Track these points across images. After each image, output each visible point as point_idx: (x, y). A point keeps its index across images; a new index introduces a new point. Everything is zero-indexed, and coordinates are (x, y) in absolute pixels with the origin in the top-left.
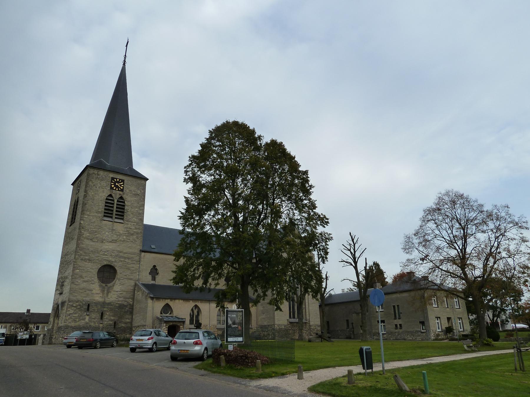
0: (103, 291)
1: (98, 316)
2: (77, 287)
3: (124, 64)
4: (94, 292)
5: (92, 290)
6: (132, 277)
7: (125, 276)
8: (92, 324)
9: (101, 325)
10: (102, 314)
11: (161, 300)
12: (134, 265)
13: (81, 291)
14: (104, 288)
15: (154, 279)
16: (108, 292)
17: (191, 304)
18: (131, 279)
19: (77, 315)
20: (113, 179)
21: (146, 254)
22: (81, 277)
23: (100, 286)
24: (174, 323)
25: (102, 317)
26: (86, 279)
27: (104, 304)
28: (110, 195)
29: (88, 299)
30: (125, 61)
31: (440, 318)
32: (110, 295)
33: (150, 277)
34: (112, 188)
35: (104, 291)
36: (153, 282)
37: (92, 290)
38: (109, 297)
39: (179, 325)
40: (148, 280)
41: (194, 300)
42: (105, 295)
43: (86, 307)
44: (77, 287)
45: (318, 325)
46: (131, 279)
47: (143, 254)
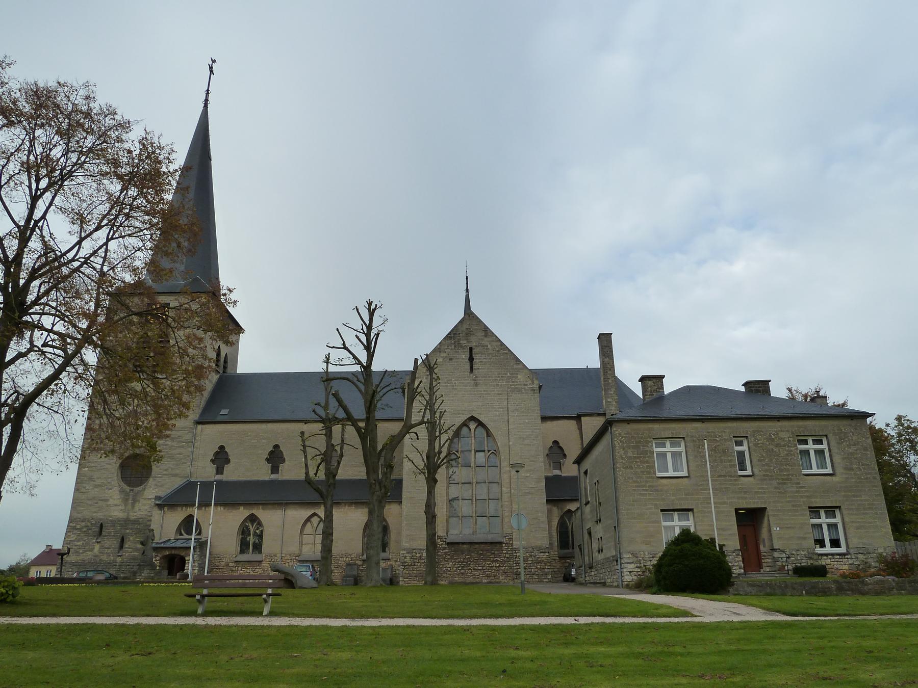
0: (125, 500)
1: (116, 543)
2: (84, 497)
3: (206, 106)
4: (111, 502)
5: (107, 500)
6: (177, 472)
7: (166, 470)
8: (104, 558)
9: (119, 560)
10: (123, 540)
11: (179, 509)
12: (181, 450)
13: (90, 502)
14: (127, 494)
15: (275, 470)
16: (135, 501)
17: (242, 513)
18: (175, 475)
19: (80, 543)
21: (204, 426)
22: (91, 479)
23: (122, 491)
24: (173, 552)
25: (121, 546)
26: (98, 482)
27: (126, 522)
29: (99, 515)
30: (206, 100)
31: (839, 507)
32: (138, 506)
33: (212, 468)
35: (127, 500)
36: (274, 476)
37: (107, 500)
38: (136, 509)
39: (183, 554)
41: (247, 505)
42: (130, 507)
43: (98, 529)
44: (84, 497)
45: (540, 550)
46: (175, 475)
47: (200, 427)
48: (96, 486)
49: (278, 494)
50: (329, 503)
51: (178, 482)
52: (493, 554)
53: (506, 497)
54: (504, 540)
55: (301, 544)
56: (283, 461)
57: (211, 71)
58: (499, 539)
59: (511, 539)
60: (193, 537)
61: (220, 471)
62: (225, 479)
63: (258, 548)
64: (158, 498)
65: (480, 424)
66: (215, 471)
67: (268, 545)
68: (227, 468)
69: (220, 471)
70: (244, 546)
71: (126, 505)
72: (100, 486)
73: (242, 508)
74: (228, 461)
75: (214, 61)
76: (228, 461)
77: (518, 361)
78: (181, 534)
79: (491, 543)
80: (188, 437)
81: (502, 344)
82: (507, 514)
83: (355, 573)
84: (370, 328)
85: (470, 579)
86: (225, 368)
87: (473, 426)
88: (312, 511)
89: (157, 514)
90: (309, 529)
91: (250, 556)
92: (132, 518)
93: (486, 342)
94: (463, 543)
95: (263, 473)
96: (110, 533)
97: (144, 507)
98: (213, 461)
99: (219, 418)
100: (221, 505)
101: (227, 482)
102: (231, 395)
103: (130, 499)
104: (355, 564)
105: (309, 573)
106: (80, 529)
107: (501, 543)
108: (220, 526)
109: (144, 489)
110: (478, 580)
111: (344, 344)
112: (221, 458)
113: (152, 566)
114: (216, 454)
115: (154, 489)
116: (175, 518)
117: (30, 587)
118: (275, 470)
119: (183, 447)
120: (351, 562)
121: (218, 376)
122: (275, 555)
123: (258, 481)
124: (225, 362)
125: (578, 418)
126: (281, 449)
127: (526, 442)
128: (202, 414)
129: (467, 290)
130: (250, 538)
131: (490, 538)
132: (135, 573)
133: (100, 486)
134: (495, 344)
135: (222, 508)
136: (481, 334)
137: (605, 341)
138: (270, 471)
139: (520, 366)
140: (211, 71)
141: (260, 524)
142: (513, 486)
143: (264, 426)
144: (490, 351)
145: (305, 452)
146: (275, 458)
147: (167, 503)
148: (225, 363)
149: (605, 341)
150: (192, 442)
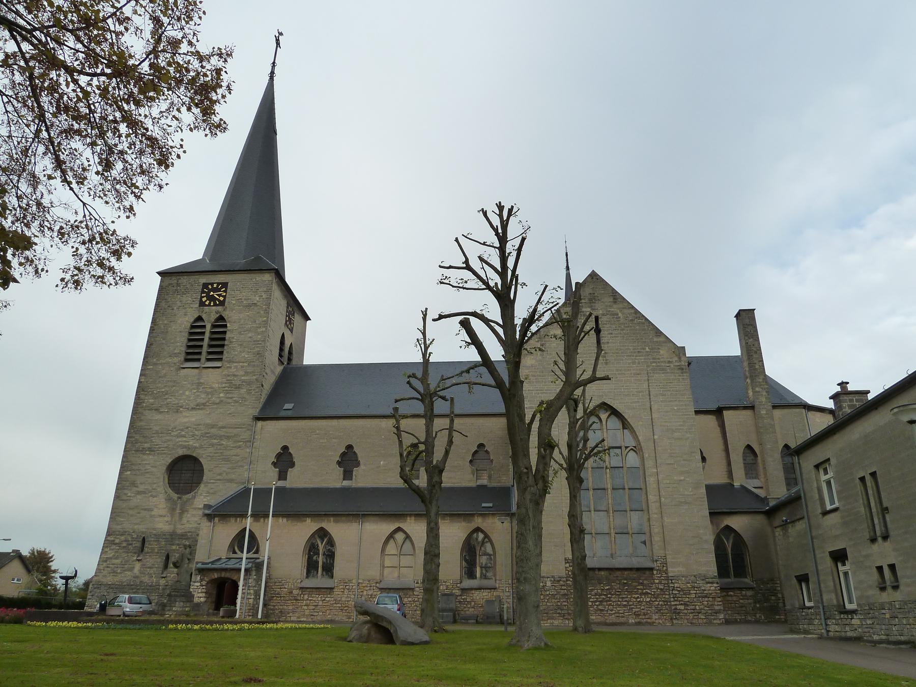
0: (172, 510)
4: (155, 512)
5: (150, 510)
6: (233, 476)
7: (220, 474)
8: (146, 579)
9: (162, 582)
11: (233, 520)
15: (348, 475)
17: (309, 527)
18: (231, 481)
20: (205, 285)
22: (134, 484)
23: (169, 499)
24: (223, 575)
26: (141, 488)
27: (173, 536)
28: (200, 319)
29: (142, 528)
30: (272, 73)
34: (202, 304)
36: (346, 483)
37: (150, 510)
38: (185, 520)
40: (267, 477)
41: (316, 515)
42: (177, 517)
43: (139, 544)
46: (231, 481)
47: (260, 423)
48: (139, 493)
49: (355, 504)
50: (433, 510)
51: (233, 489)
52: (642, 584)
53: (654, 507)
54: (655, 565)
55: (383, 567)
56: (358, 464)
57: (278, 44)
58: (649, 564)
59: (665, 564)
60: (245, 555)
61: (282, 476)
62: (288, 486)
63: (329, 570)
64: (207, 506)
65: (614, 412)
66: (276, 476)
67: (341, 567)
68: (292, 473)
69: (282, 476)
70: (311, 567)
71: (172, 516)
72: (144, 493)
73: (309, 520)
74: (292, 465)
75: (281, 34)
76: (292, 465)
77: (659, 333)
78: (234, 552)
79: (638, 569)
80: (246, 435)
81: (637, 312)
82: (656, 530)
83: (452, 606)
84: (503, 239)
85: (612, 618)
86: (290, 360)
87: (604, 416)
88: (396, 525)
89: (206, 525)
90: (391, 548)
91: (320, 580)
92: (179, 531)
93: (615, 309)
94: (600, 569)
95: (333, 479)
96: (153, 549)
97: (192, 519)
98: (274, 464)
99: (283, 414)
100: (283, 516)
101: (292, 489)
102: (293, 388)
103: (177, 509)
104: (451, 595)
105: (396, 607)
106: (118, 544)
107: (652, 569)
108: (282, 543)
109: (194, 497)
110: (622, 620)
111: (467, 261)
112: (284, 460)
113: (189, 597)
114: (279, 456)
115: (206, 496)
116: (226, 532)
117: (17, 626)
118: (348, 475)
119: (239, 447)
120: (447, 592)
121: (282, 368)
122: (350, 581)
123: (327, 489)
124: (290, 353)
125: (718, 412)
126: (355, 449)
127: (676, 435)
128: (263, 409)
129: (568, 268)
130: (320, 557)
131: (635, 562)
132: (163, 606)
133: (144, 493)
134: (626, 311)
135: (285, 520)
136: (608, 300)
137: (746, 321)
138: (342, 476)
139: (662, 339)
140: (278, 44)
141: (331, 543)
142: (663, 493)
143: (335, 422)
144: (622, 320)
145: (399, 436)
146: (348, 460)
147: (218, 513)
148: (289, 354)
149: (746, 321)
150: (251, 442)
